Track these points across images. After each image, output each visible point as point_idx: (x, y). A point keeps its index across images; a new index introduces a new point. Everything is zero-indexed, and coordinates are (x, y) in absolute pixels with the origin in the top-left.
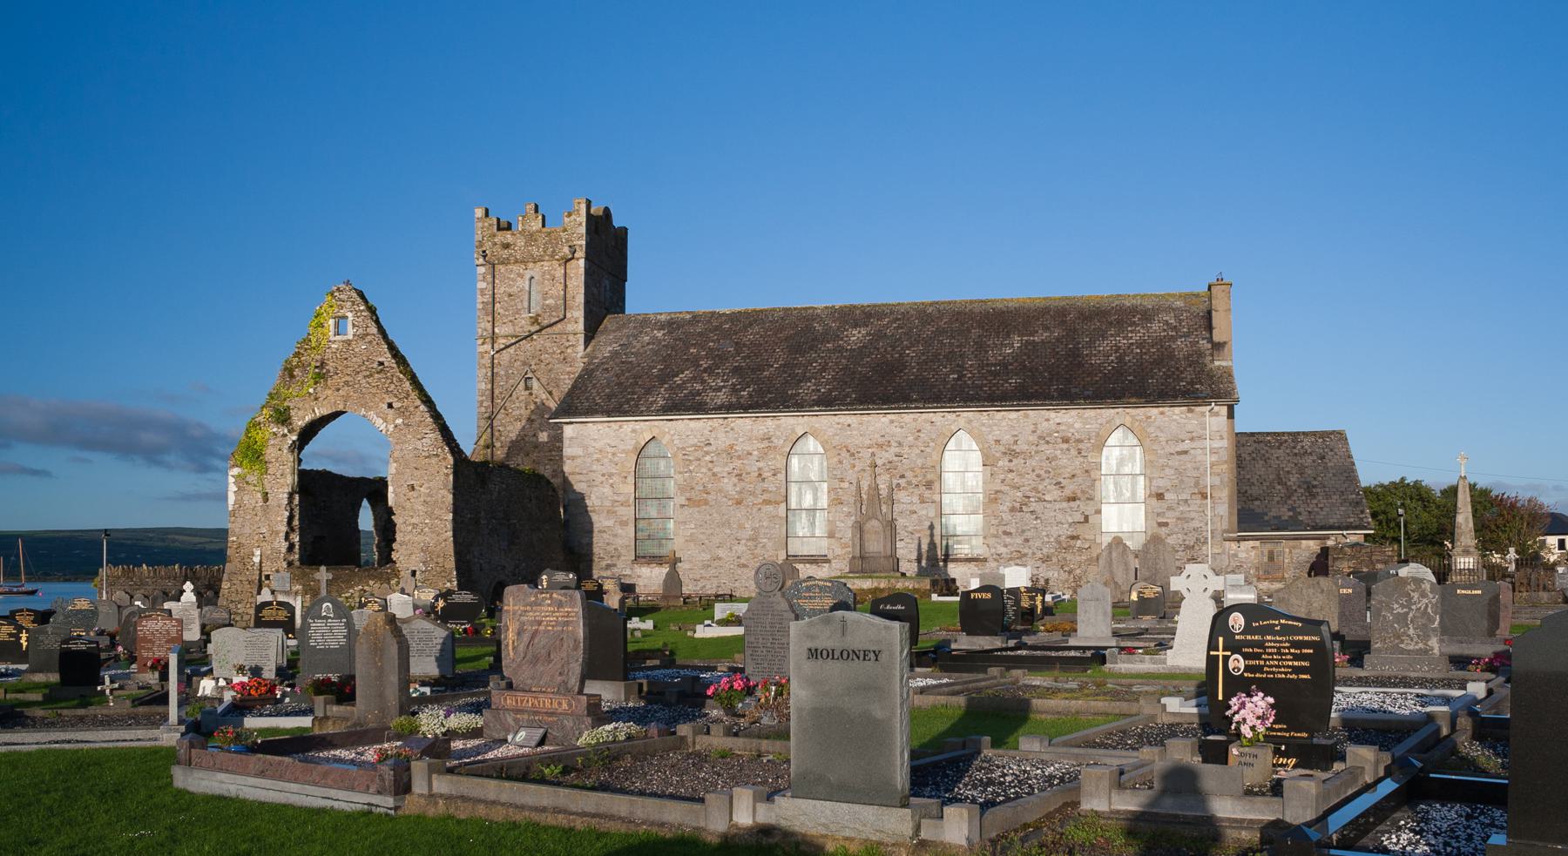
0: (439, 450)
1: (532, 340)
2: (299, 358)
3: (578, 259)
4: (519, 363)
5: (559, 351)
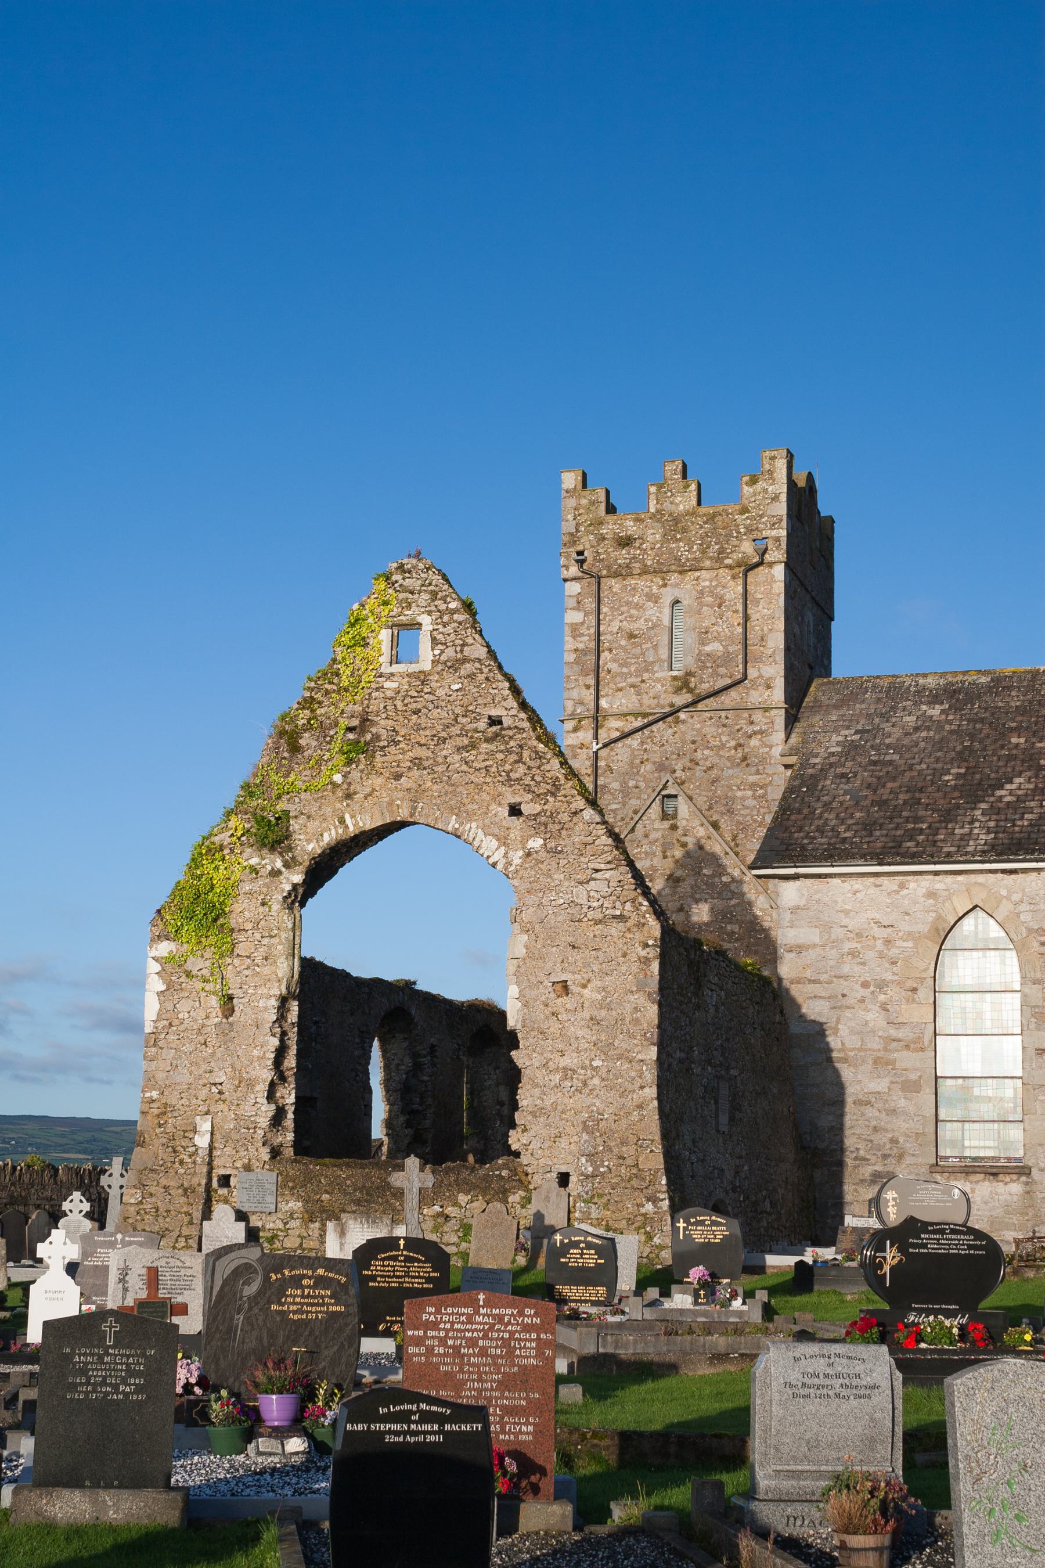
0: (628, 906)
1: (677, 721)
2: (313, 711)
3: (771, 565)
4: (649, 767)
5: (733, 743)
